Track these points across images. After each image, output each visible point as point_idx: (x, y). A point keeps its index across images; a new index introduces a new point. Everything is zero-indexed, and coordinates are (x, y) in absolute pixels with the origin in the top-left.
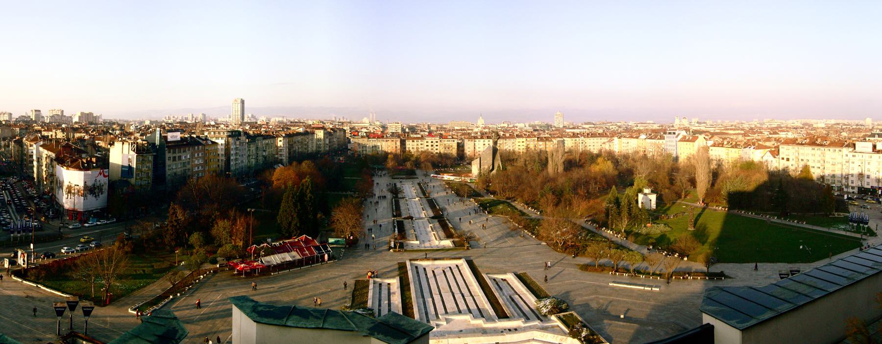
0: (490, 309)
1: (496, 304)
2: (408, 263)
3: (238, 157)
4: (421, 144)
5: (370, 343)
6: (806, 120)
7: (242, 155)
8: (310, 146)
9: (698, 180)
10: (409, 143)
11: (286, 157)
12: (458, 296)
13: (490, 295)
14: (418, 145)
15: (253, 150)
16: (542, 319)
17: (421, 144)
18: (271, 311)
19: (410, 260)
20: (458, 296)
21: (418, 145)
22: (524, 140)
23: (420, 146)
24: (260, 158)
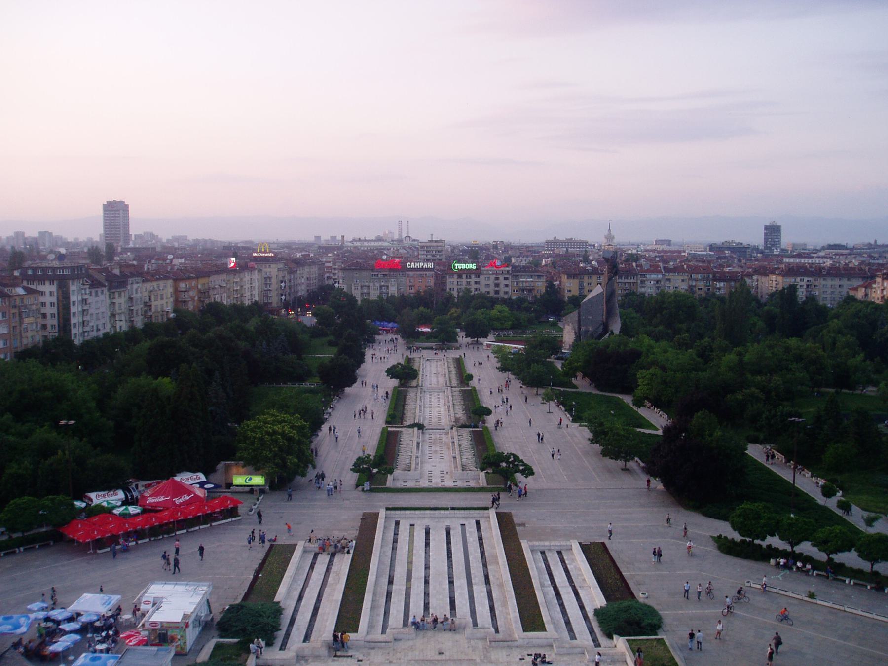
0: (516, 622)
1: (495, 620)
2: (382, 513)
3: (87, 318)
4: (476, 283)
5: (7, 548)
6: (762, 263)
7: (104, 317)
8: (247, 294)
9: (54, 611)
10: (451, 280)
11: (126, 321)
12: (460, 583)
13: (472, 608)
14: (468, 283)
15: (137, 310)
16: (9, 616)
17: (476, 283)
18: (52, 495)
19: (387, 509)
20: (460, 583)
21: (468, 283)
22: (685, 277)
23: (473, 287)
24: (635, 279)
